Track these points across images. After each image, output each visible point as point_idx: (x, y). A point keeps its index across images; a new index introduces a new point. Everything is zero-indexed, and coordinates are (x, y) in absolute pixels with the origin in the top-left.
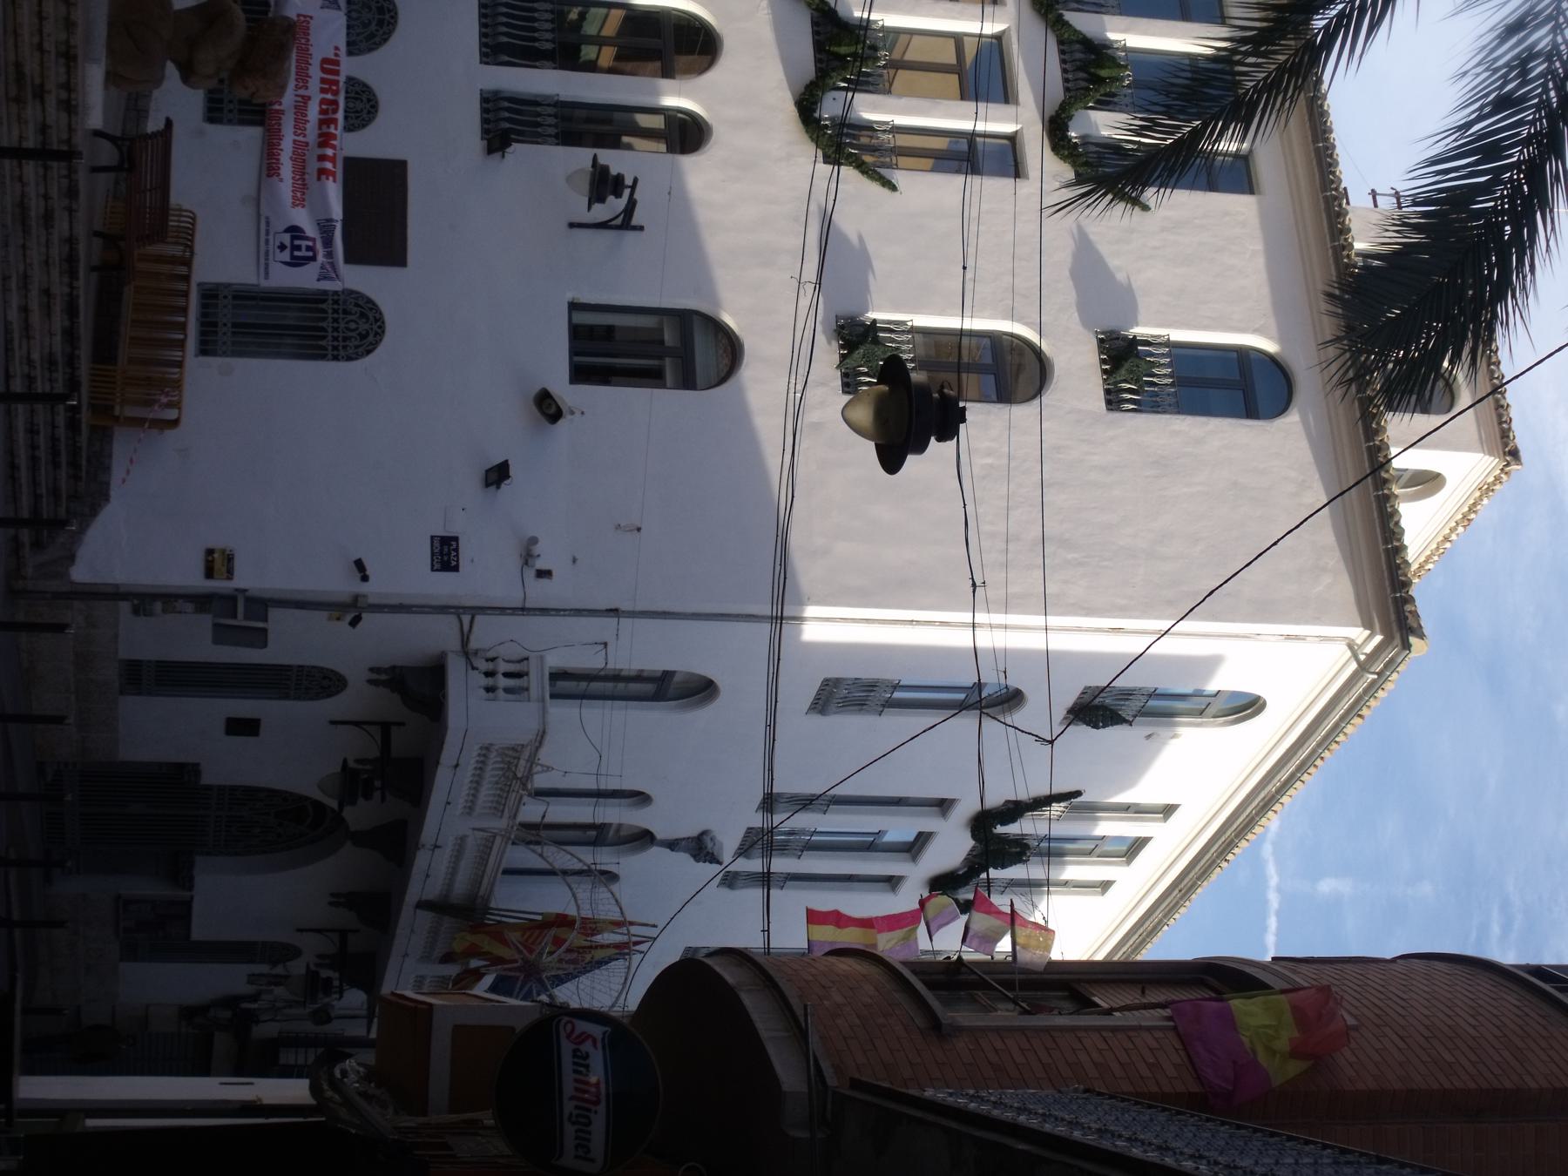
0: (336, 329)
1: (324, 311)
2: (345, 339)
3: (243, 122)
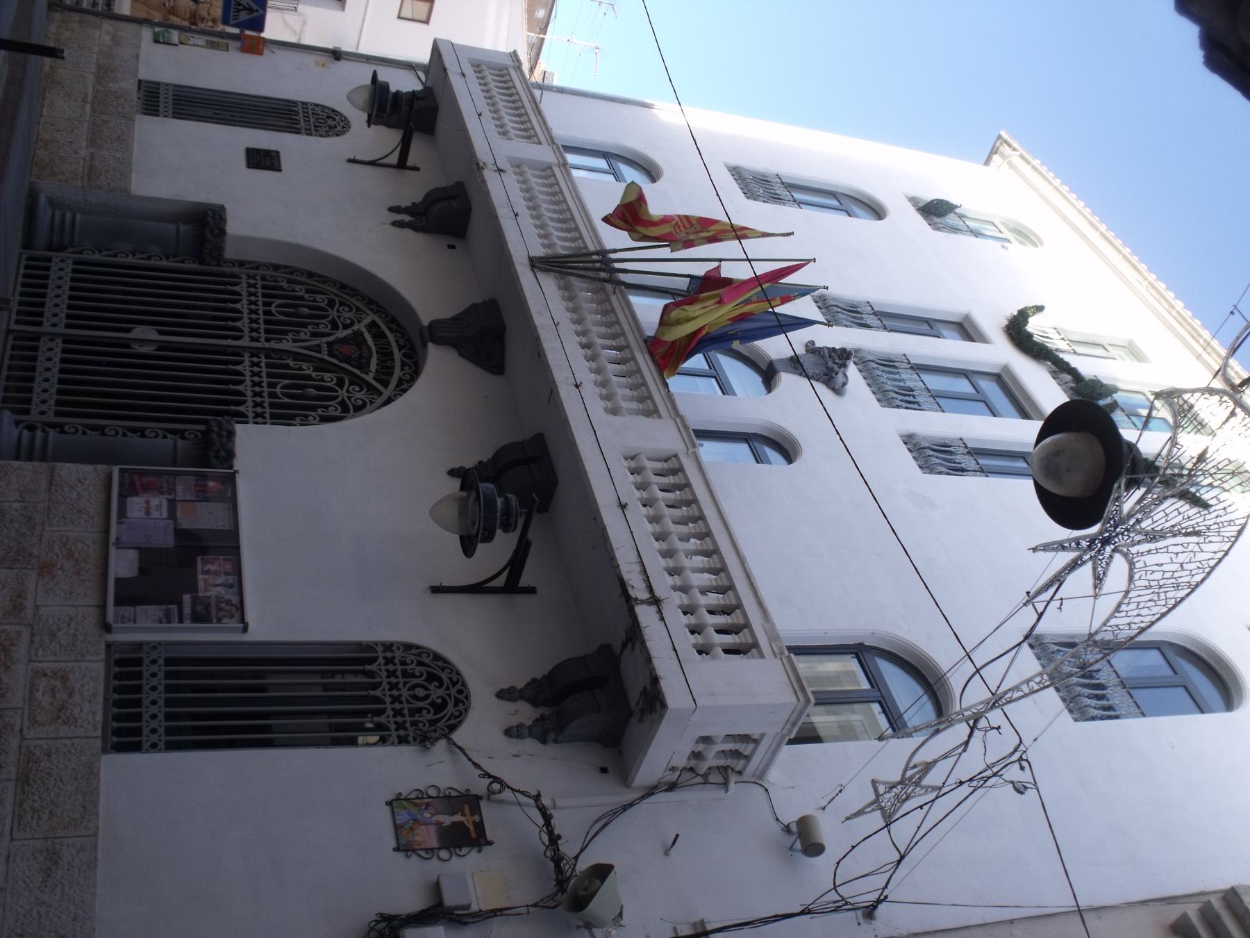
0: (396, 699)
3: (228, 457)
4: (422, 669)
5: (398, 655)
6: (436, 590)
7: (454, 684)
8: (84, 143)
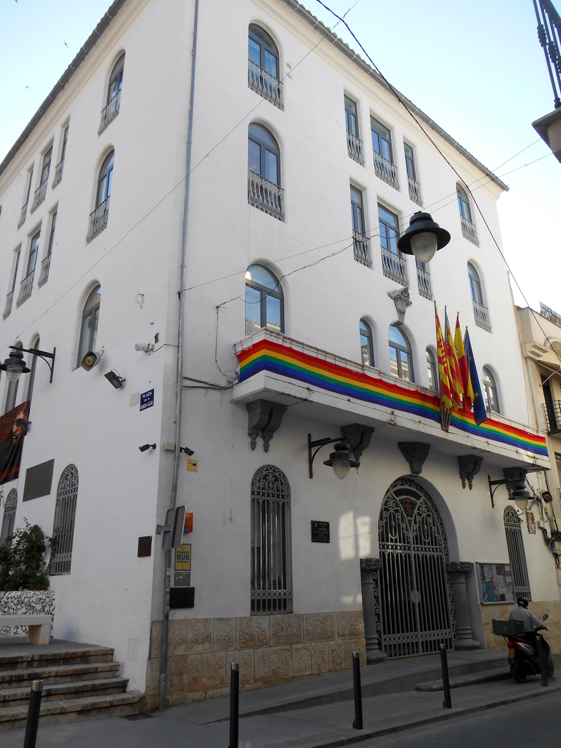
1: (264, 502)
4: (262, 481)
5: (256, 489)
6: (311, 476)
7: (267, 470)
8: (331, 643)
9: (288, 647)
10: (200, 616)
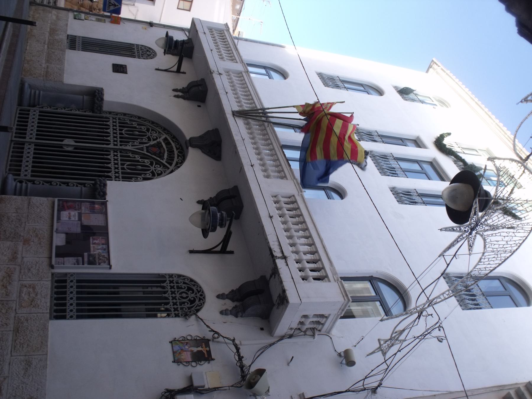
0: (174, 298)
1: (166, 298)
2: (181, 304)
5: (175, 279)
6: (191, 252)
7: (199, 292)
8: (44, 62)
9: (47, 43)
10: (69, 20)
